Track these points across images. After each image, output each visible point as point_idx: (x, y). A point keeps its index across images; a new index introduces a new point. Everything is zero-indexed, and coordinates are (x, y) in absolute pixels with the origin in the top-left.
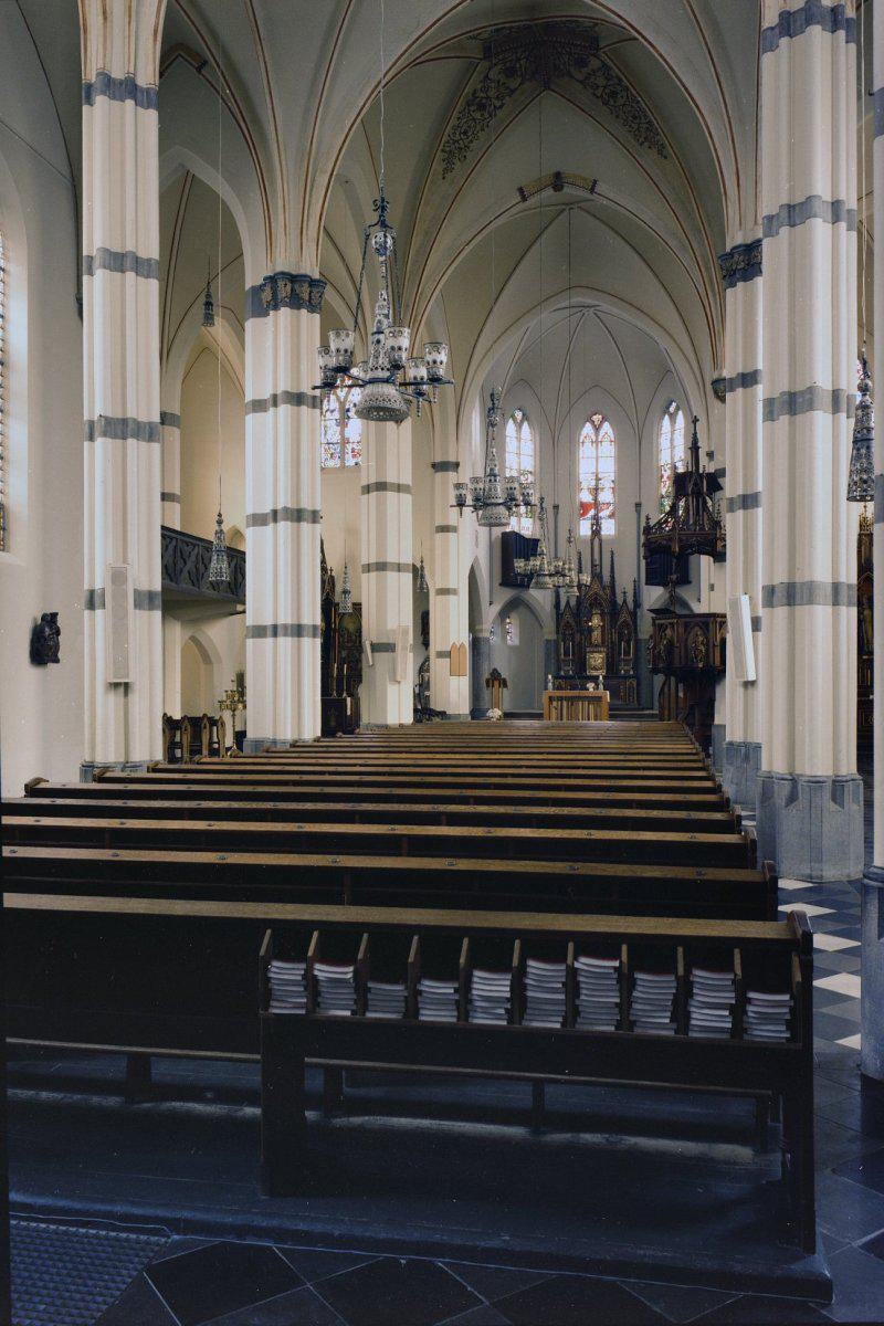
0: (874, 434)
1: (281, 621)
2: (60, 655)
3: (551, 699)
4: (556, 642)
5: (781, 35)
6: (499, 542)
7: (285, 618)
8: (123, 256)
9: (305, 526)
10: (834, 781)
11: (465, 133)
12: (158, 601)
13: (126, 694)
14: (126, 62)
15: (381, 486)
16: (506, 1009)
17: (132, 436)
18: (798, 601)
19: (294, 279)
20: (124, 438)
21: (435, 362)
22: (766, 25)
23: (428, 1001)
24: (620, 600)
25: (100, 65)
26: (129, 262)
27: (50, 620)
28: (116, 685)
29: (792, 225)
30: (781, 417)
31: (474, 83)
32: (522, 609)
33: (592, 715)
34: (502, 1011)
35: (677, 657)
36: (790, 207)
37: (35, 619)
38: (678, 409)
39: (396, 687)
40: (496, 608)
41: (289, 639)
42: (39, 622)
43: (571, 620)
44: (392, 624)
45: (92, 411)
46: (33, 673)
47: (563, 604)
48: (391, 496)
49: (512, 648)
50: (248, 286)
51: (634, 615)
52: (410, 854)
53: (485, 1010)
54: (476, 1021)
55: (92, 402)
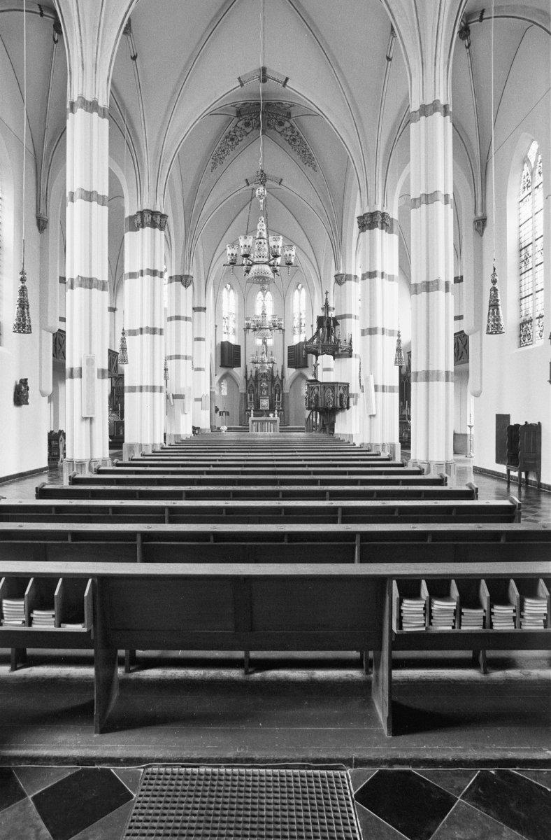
0: (499, 303)
1: (144, 384)
2: (29, 401)
3: (253, 421)
4: (246, 395)
5: (421, 115)
6: (220, 345)
7: (147, 382)
8: (91, 193)
9: (157, 336)
10: (446, 464)
11: (223, 151)
12: (107, 375)
13: (91, 423)
14: (94, 92)
15: (178, 318)
16: (544, 620)
17: (95, 287)
18: (430, 379)
19: (153, 213)
20: (90, 288)
21: (290, 255)
22: (412, 110)
23: (497, 618)
24: (275, 375)
25: (80, 93)
26: (94, 196)
27: (24, 382)
28: (86, 418)
29: (427, 204)
30: (423, 293)
31: (231, 128)
32: (228, 378)
33: (272, 430)
34: (542, 621)
35: (320, 402)
36: (427, 196)
37: (16, 382)
38: (302, 287)
39: (184, 416)
40: (218, 378)
41: (149, 393)
42: (18, 383)
43: (253, 383)
44: (182, 385)
45: (72, 273)
46: (16, 409)
47: (249, 377)
48: (182, 322)
49: (224, 397)
50: (127, 214)
51: (282, 382)
52: (136, 491)
53: (531, 621)
54: (526, 628)
55: (72, 267)
